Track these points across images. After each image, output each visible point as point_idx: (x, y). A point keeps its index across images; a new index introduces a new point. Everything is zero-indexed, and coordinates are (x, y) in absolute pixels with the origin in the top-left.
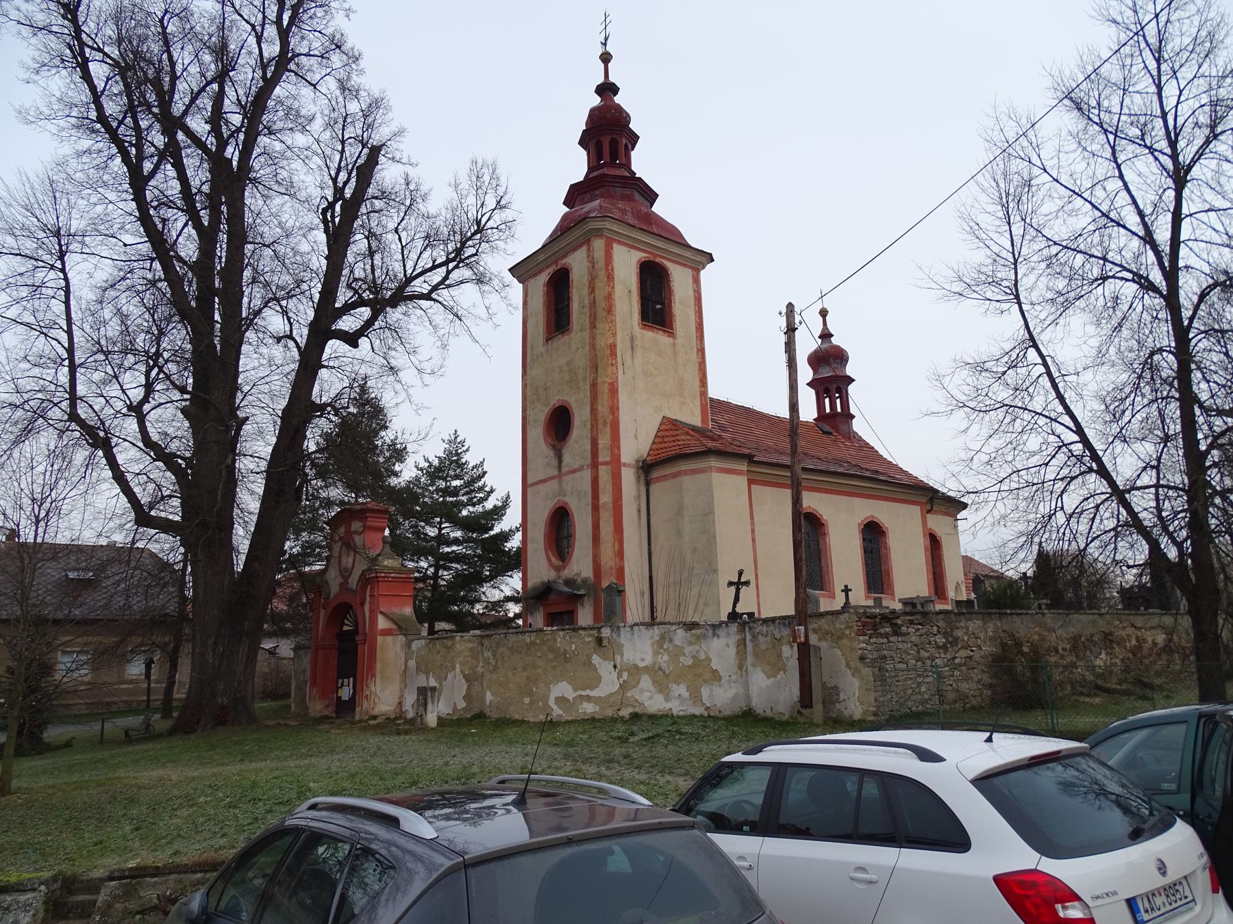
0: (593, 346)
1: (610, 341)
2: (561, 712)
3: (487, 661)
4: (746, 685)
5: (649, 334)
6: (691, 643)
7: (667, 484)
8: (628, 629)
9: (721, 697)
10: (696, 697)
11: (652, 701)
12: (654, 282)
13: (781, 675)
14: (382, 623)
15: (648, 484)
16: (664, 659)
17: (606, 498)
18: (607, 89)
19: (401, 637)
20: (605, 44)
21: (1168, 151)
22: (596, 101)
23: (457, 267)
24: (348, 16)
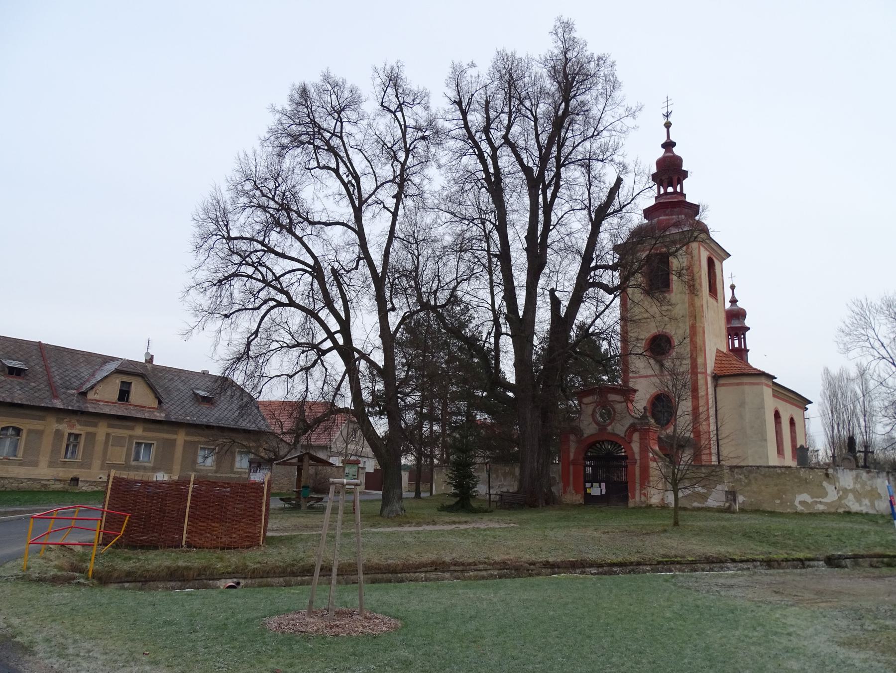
7: (731, 388)
11: (854, 506)
16: (858, 486)
18: (669, 145)
20: (667, 116)
21: (531, 160)
22: (661, 152)
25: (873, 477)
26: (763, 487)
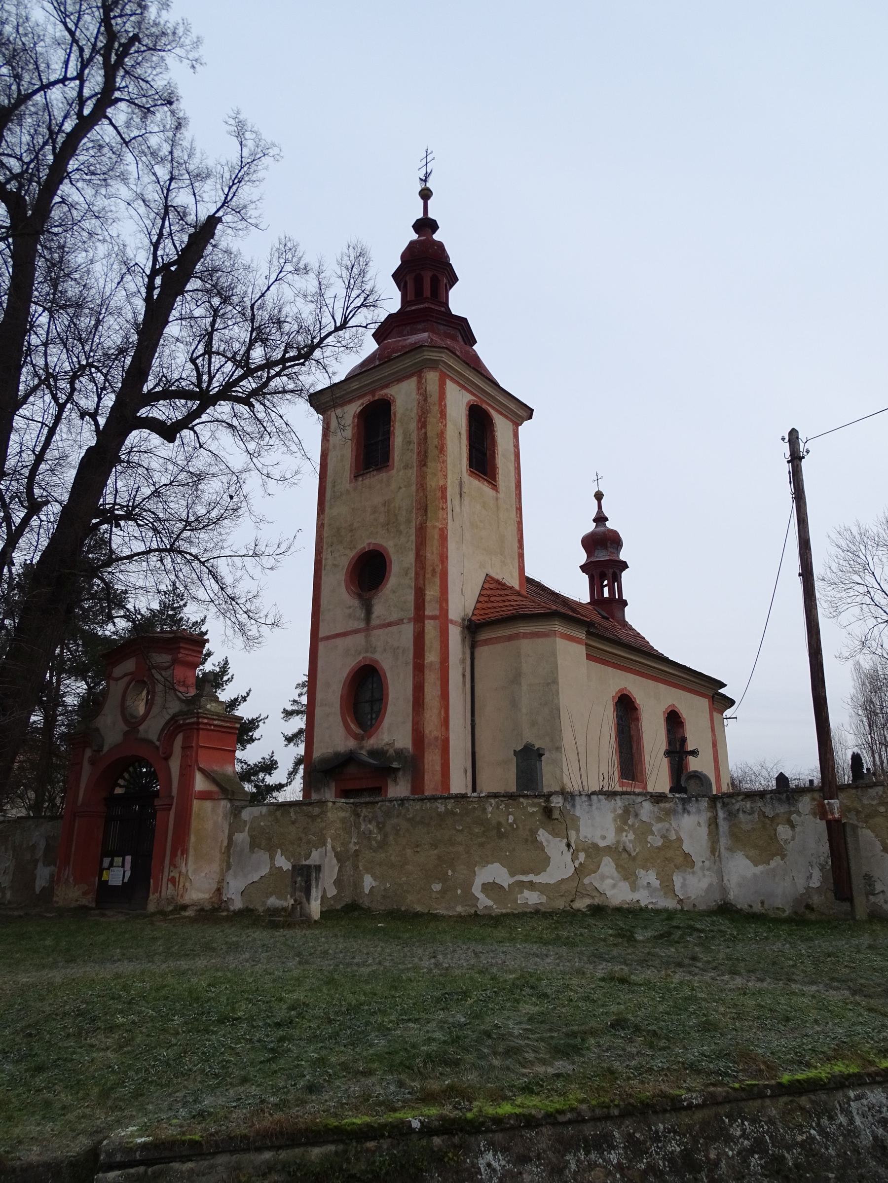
0: (422, 486)
1: (441, 483)
2: (490, 903)
3: (366, 837)
4: (720, 874)
5: (476, 483)
6: (659, 820)
7: (499, 647)
8: (584, 798)
9: (695, 886)
10: (668, 887)
11: (617, 891)
12: (480, 425)
13: (776, 862)
14: (200, 783)
15: (473, 647)
16: (628, 838)
17: (432, 657)
18: (425, 226)
19: (223, 803)
20: (425, 181)
23: (278, 374)
24: (193, 67)
25: (669, 813)
26: (409, 852)
